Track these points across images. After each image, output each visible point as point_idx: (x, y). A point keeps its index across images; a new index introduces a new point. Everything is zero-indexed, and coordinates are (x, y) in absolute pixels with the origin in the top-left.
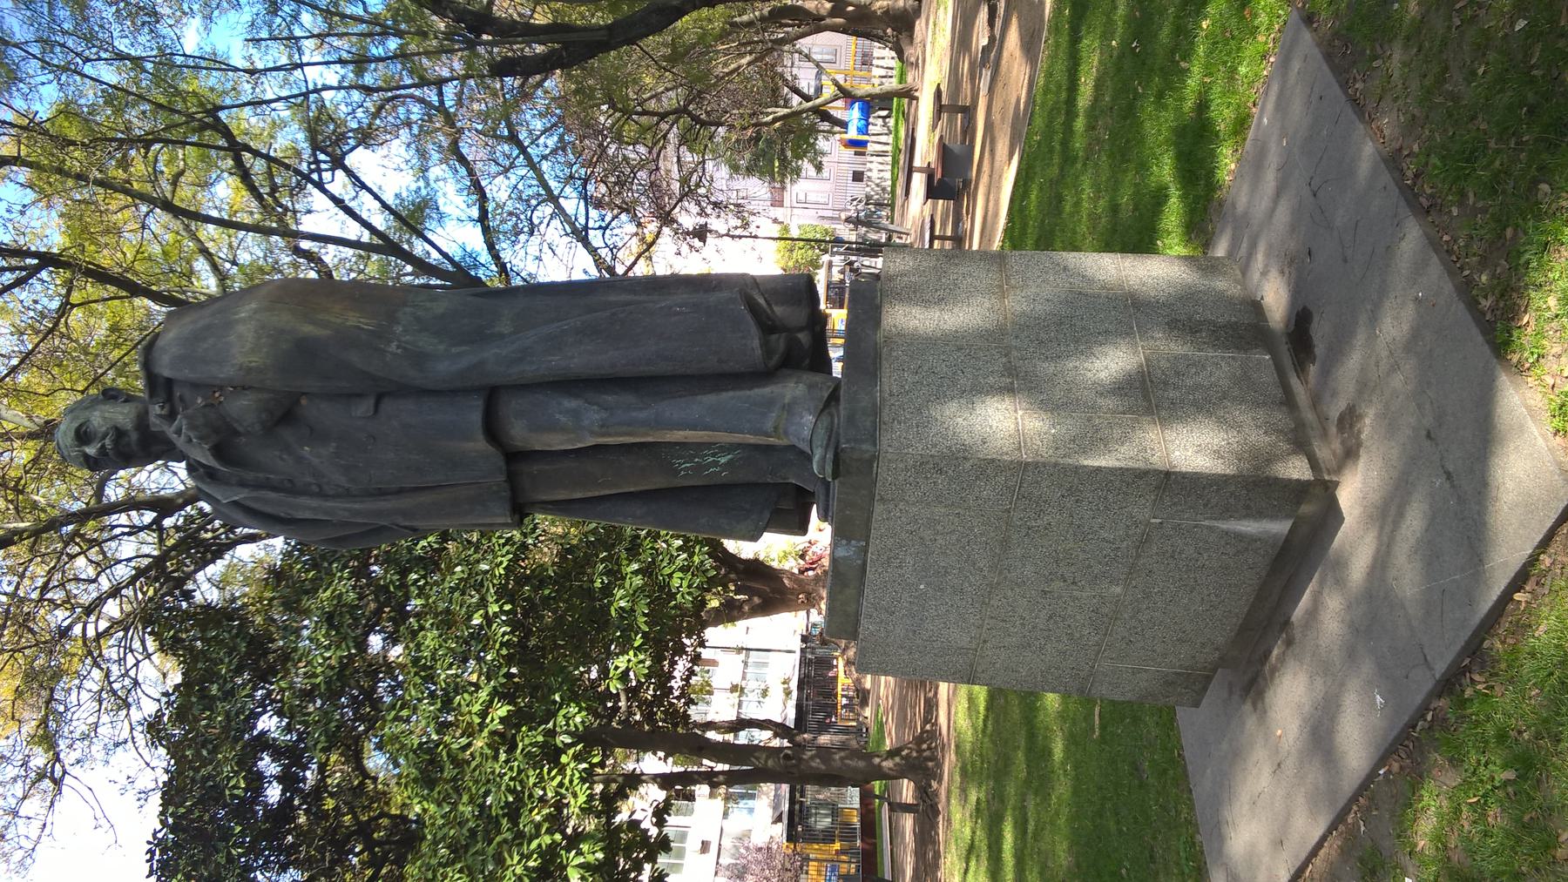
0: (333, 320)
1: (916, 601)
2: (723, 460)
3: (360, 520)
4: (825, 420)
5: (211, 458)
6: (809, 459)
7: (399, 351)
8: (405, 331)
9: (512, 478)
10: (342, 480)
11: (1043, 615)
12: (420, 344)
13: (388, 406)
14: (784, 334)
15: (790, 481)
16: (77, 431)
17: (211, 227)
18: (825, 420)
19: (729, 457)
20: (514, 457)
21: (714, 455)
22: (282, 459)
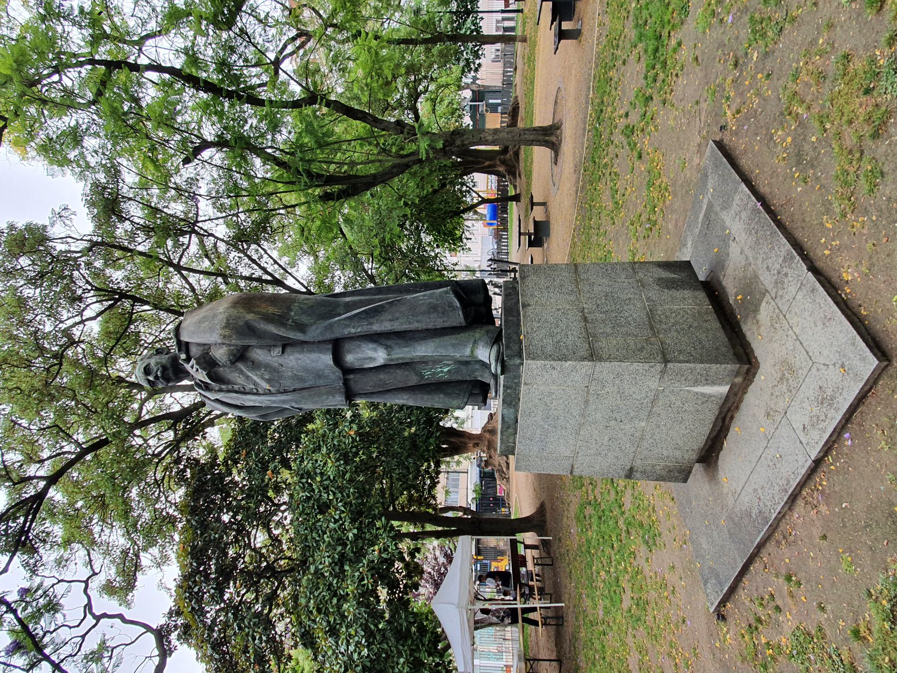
2: (445, 370)
3: (275, 405)
4: (495, 348)
6: (490, 365)
8: (295, 314)
9: (346, 382)
10: (266, 386)
11: (606, 438)
13: (288, 350)
16: (145, 368)
18: (495, 348)
20: (347, 371)
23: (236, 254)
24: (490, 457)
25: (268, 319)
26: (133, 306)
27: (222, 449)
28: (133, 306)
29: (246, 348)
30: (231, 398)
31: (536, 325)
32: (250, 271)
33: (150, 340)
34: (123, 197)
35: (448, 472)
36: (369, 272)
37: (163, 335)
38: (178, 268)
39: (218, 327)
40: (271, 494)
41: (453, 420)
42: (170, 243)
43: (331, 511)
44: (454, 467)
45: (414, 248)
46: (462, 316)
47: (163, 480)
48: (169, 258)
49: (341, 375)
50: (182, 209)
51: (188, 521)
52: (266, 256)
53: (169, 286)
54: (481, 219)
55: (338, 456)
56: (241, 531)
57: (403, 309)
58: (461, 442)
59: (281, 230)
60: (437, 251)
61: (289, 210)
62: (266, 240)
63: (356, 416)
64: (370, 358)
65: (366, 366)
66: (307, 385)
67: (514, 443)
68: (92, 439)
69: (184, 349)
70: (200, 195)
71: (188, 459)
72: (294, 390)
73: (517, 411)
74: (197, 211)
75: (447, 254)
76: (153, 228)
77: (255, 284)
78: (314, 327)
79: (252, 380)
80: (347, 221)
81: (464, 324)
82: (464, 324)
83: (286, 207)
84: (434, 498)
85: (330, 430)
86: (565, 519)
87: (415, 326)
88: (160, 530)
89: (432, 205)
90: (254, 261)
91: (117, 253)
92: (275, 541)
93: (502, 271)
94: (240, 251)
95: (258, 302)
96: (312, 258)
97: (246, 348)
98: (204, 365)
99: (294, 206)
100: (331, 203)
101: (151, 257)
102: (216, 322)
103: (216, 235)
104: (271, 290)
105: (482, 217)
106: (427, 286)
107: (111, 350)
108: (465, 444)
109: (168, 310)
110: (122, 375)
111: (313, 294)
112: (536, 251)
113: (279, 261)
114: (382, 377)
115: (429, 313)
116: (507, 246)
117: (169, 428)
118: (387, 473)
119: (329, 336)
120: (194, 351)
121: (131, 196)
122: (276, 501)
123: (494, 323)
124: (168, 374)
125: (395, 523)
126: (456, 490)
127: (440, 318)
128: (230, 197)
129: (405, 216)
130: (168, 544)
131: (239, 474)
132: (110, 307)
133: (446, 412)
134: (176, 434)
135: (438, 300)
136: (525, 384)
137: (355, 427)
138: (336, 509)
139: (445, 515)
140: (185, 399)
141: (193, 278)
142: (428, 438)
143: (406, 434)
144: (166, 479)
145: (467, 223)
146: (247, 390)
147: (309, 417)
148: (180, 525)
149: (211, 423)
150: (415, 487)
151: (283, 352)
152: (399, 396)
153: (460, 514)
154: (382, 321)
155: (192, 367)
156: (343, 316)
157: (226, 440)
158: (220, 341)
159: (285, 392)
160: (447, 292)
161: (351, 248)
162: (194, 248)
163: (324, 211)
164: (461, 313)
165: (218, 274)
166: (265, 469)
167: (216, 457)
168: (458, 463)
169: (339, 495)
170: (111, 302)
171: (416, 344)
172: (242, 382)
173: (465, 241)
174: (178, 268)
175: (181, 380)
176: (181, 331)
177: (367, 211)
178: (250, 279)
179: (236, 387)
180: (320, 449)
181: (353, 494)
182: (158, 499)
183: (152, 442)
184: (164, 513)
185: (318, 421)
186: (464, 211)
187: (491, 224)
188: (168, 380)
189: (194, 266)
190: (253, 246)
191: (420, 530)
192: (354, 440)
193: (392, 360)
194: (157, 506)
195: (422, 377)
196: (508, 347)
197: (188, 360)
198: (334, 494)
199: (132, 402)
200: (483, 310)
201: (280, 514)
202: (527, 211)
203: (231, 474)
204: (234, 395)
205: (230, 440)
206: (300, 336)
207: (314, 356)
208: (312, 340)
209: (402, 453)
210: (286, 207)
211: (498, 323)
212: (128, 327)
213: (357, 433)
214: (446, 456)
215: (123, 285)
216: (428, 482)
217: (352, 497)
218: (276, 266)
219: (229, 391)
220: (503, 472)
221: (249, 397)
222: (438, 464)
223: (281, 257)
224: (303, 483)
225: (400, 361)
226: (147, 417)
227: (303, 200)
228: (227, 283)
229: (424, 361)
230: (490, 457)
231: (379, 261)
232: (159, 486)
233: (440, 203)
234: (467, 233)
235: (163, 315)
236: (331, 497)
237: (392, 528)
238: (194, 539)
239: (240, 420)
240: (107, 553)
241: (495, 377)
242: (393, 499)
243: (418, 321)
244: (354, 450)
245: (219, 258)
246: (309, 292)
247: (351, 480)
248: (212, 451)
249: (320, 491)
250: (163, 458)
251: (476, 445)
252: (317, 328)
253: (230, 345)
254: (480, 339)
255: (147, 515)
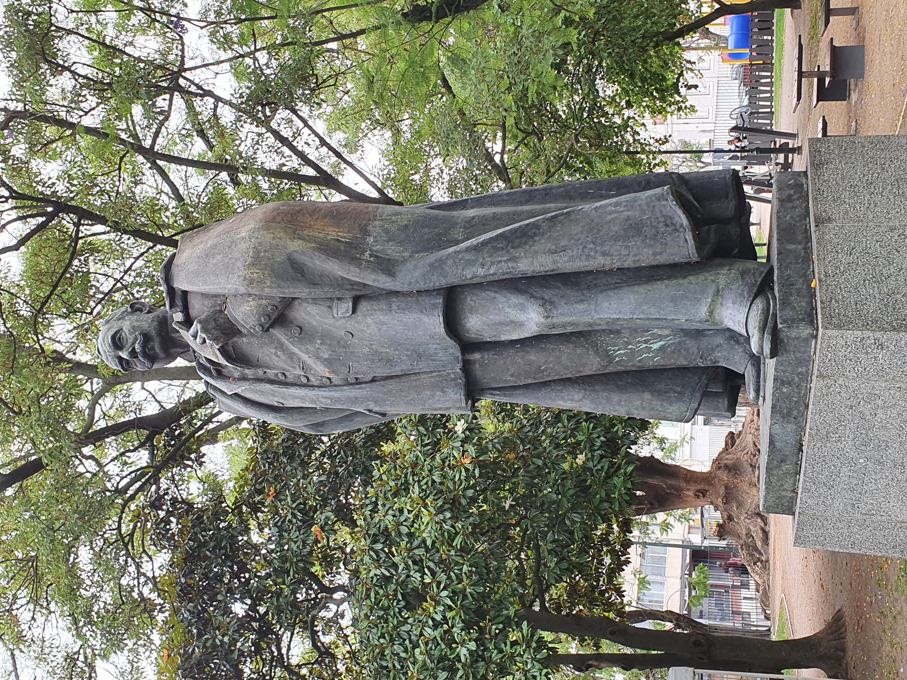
0: (317, 235)
1: (855, 475)
2: (655, 346)
4: (759, 304)
5: (220, 356)
6: (748, 340)
7: (372, 259)
9: (467, 367)
10: (323, 371)
12: (389, 252)
13: (364, 306)
14: (713, 226)
15: (720, 364)
16: (113, 337)
17: (266, 21)
18: (759, 304)
19: (662, 343)
20: (468, 346)
21: (646, 342)
22: (277, 356)
23: (254, 128)
24: (730, 518)
25: (330, 250)
26: (77, 225)
27: (231, 484)
28: (77, 225)
29: (289, 303)
30: (262, 393)
31: (845, 259)
32: (278, 160)
33: (106, 288)
34: (59, 29)
35: (644, 544)
36: (497, 158)
37: (128, 279)
38: (151, 155)
39: (239, 264)
40: (316, 569)
41: (654, 444)
42: (137, 110)
43: (428, 605)
44: (656, 534)
45: (582, 109)
46: (691, 243)
47: (131, 535)
48: (135, 136)
49: (459, 354)
50: (156, 47)
51: (176, 611)
52: (306, 131)
53: (137, 190)
54: (717, 47)
55: (440, 502)
56: (265, 632)
57: (575, 229)
58: (670, 487)
59: (332, 82)
60: (627, 113)
61: (347, 41)
62: (307, 101)
63: (473, 429)
64: (512, 322)
65: (504, 338)
66: (397, 370)
67: (795, 491)
68: (16, 460)
69: (179, 302)
70: (189, 20)
71: (174, 500)
72: (373, 380)
73: (803, 429)
74: (183, 51)
75: (648, 119)
76: (109, 84)
77: (286, 184)
78: (409, 265)
79: (299, 359)
80: (456, 60)
81: (695, 258)
82: (695, 258)
83: (341, 37)
84: (620, 594)
85: (425, 454)
86: (887, 648)
87: (598, 262)
88: (129, 623)
89: (619, 22)
90: (284, 141)
91: (50, 131)
92: (325, 654)
93: (758, 150)
94: (260, 123)
95: (309, 221)
96: (388, 134)
97: (289, 303)
98: (216, 333)
99: (354, 35)
100: (426, 26)
101: (106, 135)
102: (236, 255)
103: (217, 92)
104: (314, 195)
105: (719, 42)
106: (621, 187)
107: (43, 304)
108: (679, 490)
109: (138, 234)
110: (59, 348)
111: (390, 201)
112: (834, 109)
113: (328, 141)
114: (532, 357)
115: (626, 238)
116: (770, 99)
117: (142, 445)
118: (529, 541)
119: (439, 281)
120: (197, 307)
121: (71, 26)
122: (326, 582)
123: (754, 257)
124: (153, 348)
125: (548, 636)
126: (659, 578)
127: (650, 246)
128: (241, 21)
129: (565, 45)
130: (141, 650)
131: (261, 530)
132: (40, 228)
133: (644, 425)
134: (153, 456)
135: (643, 212)
136: (821, 376)
137: (471, 450)
138: (437, 603)
139: (638, 625)
140: (165, 392)
141: (175, 172)
142: (609, 476)
143: (566, 466)
144: (137, 534)
145: (688, 55)
146: (290, 378)
147: (386, 432)
148: (160, 617)
149: (212, 438)
150: (581, 568)
151: (354, 312)
152: (565, 394)
153: (669, 626)
154: (536, 252)
155: (195, 336)
156: (463, 245)
157: (238, 469)
158: (242, 290)
159: (358, 382)
160: (660, 198)
161: (462, 113)
162: (178, 118)
163: (412, 42)
164: (689, 236)
165: (219, 166)
166: (308, 523)
167: (220, 499)
168: (666, 527)
169: (443, 577)
170: (41, 219)
171: (600, 297)
172: (281, 364)
173: (683, 91)
174: (151, 155)
175: (174, 359)
176: (175, 270)
177: (492, 39)
178: (278, 174)
179: (271, 373)
180: (407, 490)
181: (469, 575)
182: (124, 570)
183: (113, 469)
184: (135, 595)
185: (401, 439)
186: (682, 33)
187: (735, 56)
188: (152, 359)
189: (176, 152)
190: (283, 113)
191: (590, 651)
192: (469, 475)
193: (554, 326)
194: (124, 582)
195: (610, 358)
196: (785, 303)
197: (188, 322)
198: (433, 574)
199: (78, 396)
200: (733, 230)
201: (333, 607)
202: (814, 26)
203: (247, 530)
204: (268, 386)
205: (247, 469)
206: (383, 282)
207: (410, 318)
208: (406, 288)
209: (558, 503)
210: (341, 37)
211: (762, 252)
212: (70, 264)
213: (475, 462)
214: (639, 512)
215: (61, 188)
216: (607, 560)
217: (466, 581)
218: (324, 150)
219: (259, 380)
220: (756, 549)
221: (293, 390)
222: (626, 527)
223: (330, 132)
224: (376, 552)
225: (569, 330)
226: (102, 424)
227: (373, 22)
228: (236, 183)
229: (613, 331)
230: (730, 518)
231: (515, 137)
232: (126, 545)
233: (636, 17)
234: (688, 75)
235: (128, 240)
236: (428, 580)
237: (541, 643)
238: (187, 644)
239: (264, 430)
240: (41, 658)
241: (756, 361)
242: (542, 589)
243: (604, 254)
244: (470, 493)
245: (222, 135)
246: (386, 200)
247: (464, 550)
248: (214, 486)
249: (407, 567)
250: (132, 498)
251: (701, 494)
252: (416, 267)
253: (260, 297)
254: (727, 285)
255: (107, 597)
